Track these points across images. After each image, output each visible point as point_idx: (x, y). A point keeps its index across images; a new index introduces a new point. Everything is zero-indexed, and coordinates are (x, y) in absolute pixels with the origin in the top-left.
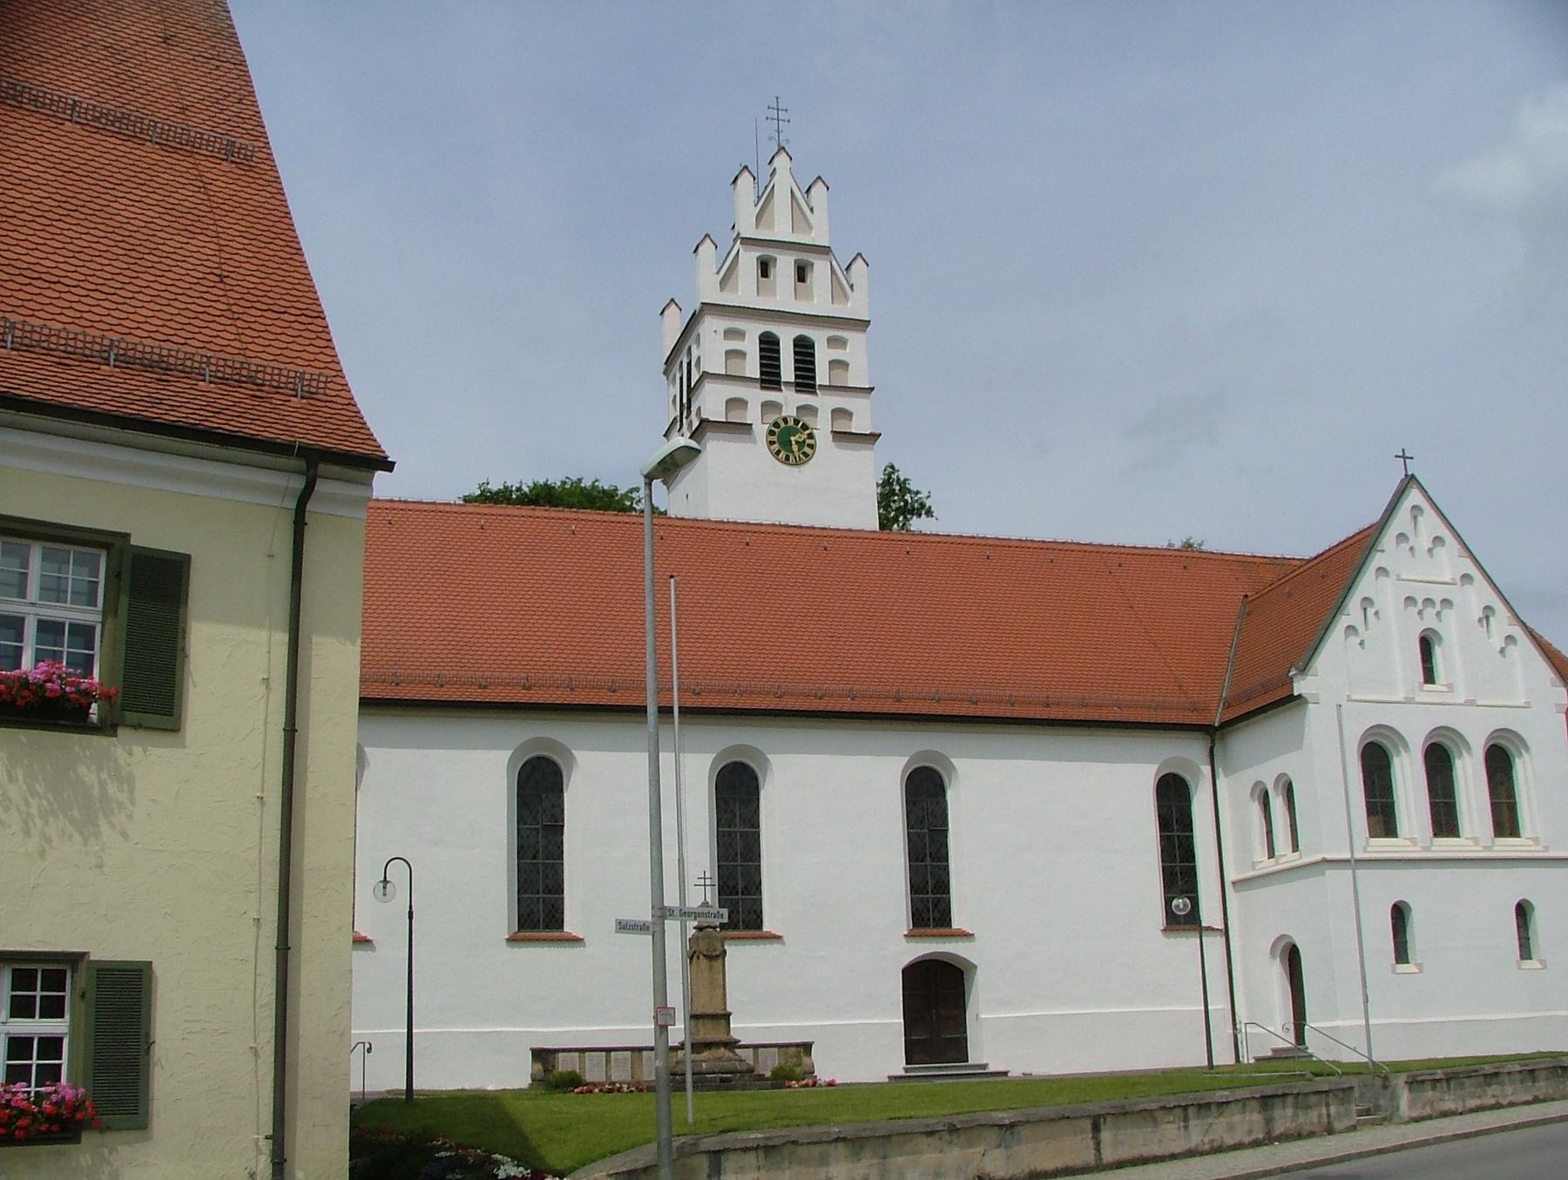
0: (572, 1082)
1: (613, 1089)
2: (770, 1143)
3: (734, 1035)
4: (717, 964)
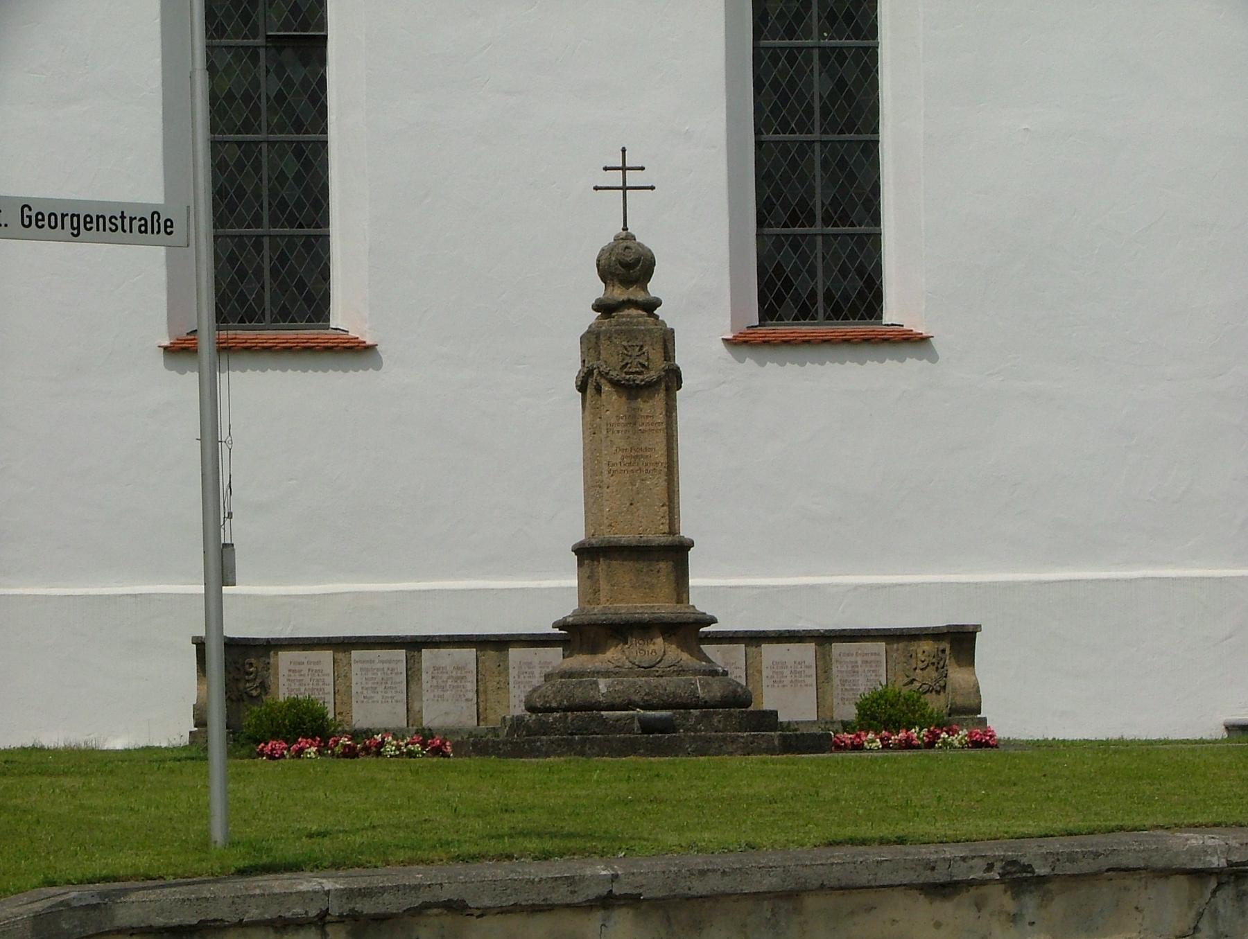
0: (306, 726)
1: (433, 744)
2: (367, 907)
3: (699, 602)
4: (652, 407)
